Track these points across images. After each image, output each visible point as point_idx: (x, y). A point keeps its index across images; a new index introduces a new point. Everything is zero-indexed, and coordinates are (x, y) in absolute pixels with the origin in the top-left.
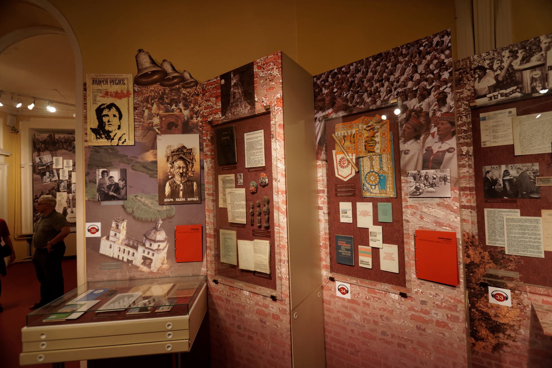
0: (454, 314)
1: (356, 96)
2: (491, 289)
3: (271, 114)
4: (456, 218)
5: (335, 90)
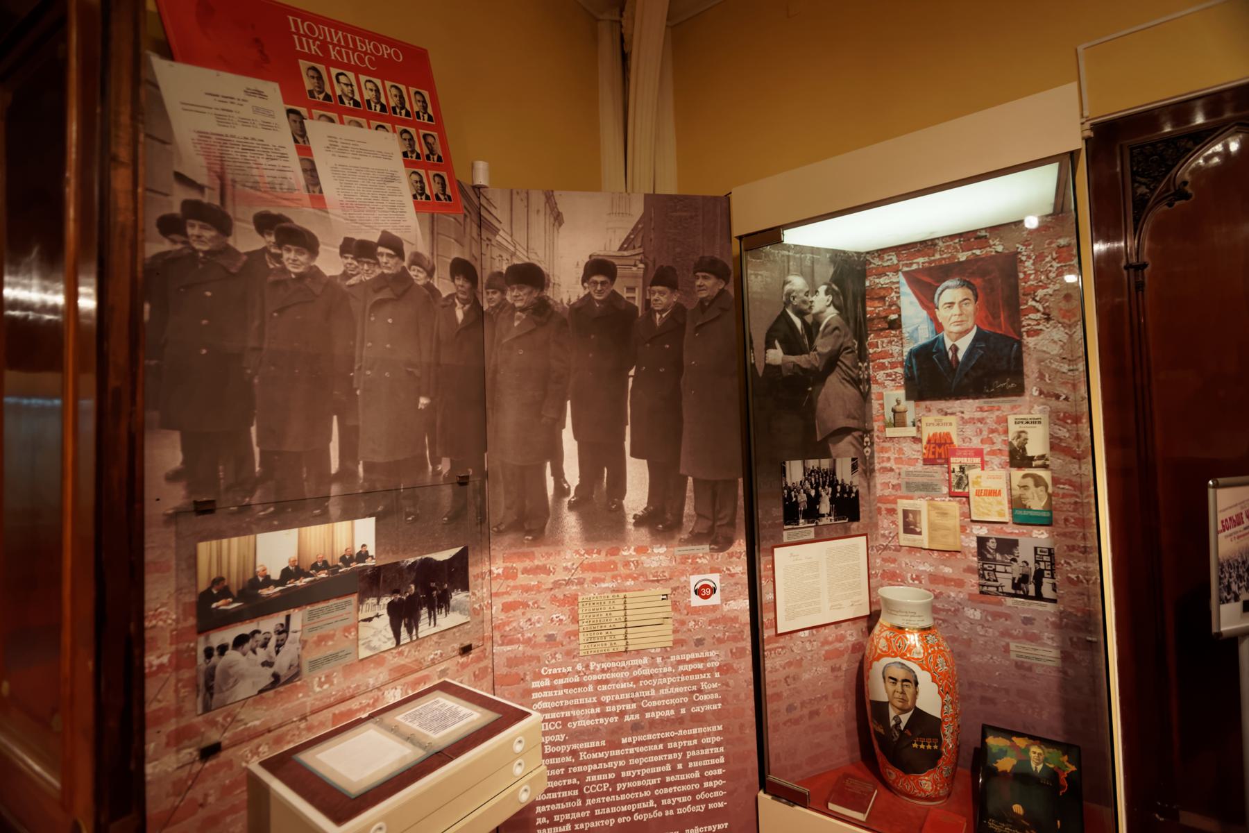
0: (740, 645)
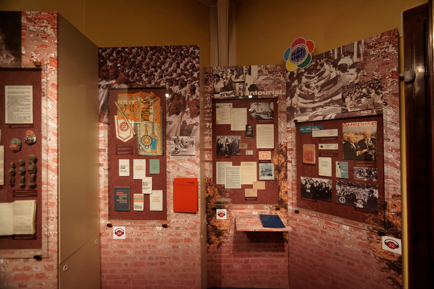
0: (195, 231)
1: (136, 74)
2: (218, 211)
3: (43, 72)
4: (54, 176)
5: (119, 65)
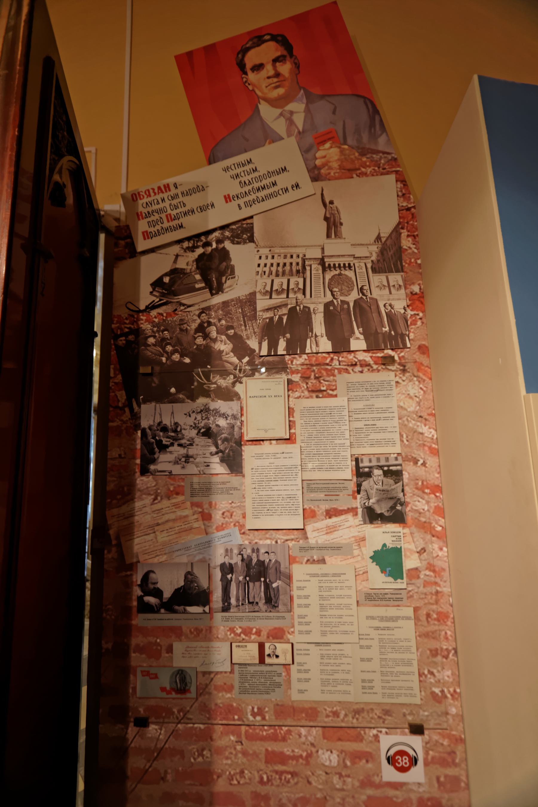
0: (451, 771)
4: (441, 549)
